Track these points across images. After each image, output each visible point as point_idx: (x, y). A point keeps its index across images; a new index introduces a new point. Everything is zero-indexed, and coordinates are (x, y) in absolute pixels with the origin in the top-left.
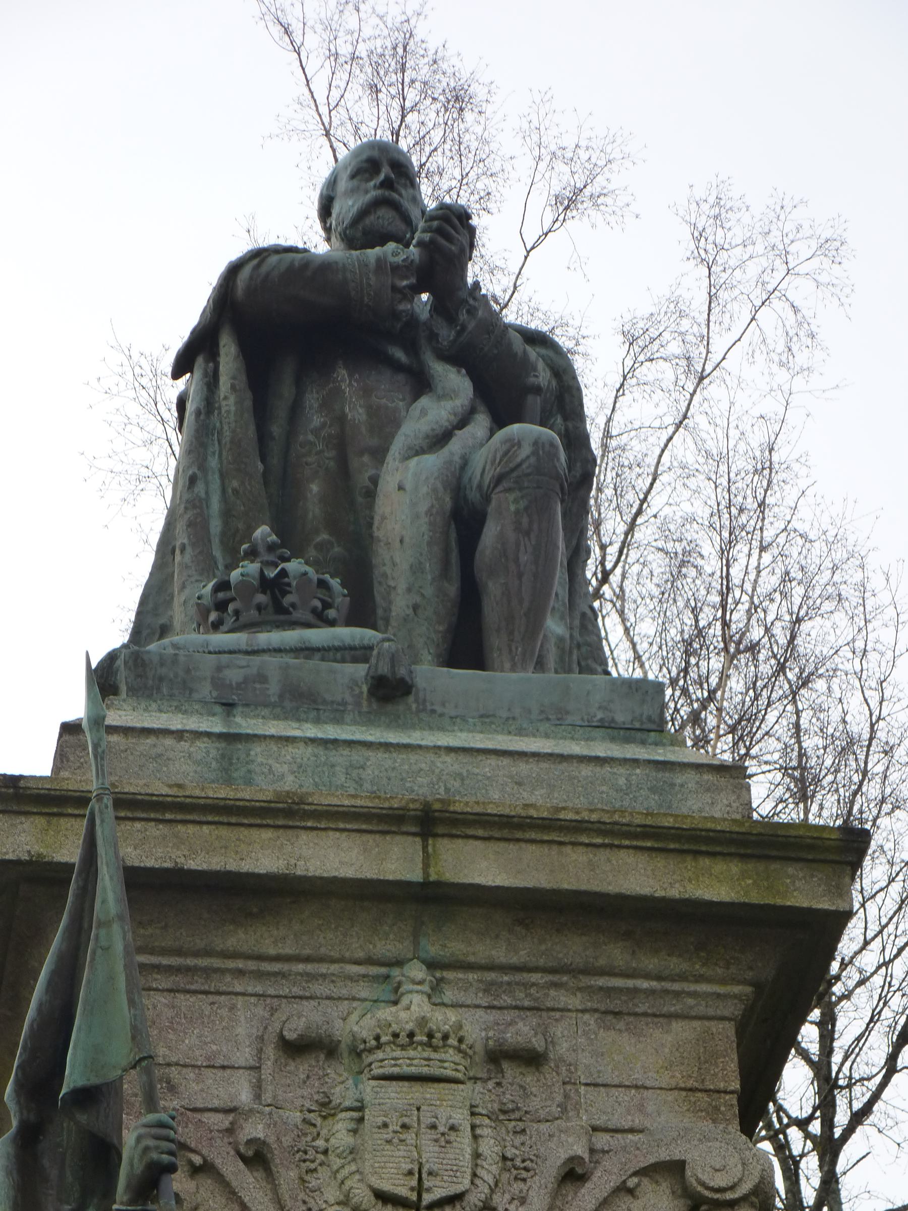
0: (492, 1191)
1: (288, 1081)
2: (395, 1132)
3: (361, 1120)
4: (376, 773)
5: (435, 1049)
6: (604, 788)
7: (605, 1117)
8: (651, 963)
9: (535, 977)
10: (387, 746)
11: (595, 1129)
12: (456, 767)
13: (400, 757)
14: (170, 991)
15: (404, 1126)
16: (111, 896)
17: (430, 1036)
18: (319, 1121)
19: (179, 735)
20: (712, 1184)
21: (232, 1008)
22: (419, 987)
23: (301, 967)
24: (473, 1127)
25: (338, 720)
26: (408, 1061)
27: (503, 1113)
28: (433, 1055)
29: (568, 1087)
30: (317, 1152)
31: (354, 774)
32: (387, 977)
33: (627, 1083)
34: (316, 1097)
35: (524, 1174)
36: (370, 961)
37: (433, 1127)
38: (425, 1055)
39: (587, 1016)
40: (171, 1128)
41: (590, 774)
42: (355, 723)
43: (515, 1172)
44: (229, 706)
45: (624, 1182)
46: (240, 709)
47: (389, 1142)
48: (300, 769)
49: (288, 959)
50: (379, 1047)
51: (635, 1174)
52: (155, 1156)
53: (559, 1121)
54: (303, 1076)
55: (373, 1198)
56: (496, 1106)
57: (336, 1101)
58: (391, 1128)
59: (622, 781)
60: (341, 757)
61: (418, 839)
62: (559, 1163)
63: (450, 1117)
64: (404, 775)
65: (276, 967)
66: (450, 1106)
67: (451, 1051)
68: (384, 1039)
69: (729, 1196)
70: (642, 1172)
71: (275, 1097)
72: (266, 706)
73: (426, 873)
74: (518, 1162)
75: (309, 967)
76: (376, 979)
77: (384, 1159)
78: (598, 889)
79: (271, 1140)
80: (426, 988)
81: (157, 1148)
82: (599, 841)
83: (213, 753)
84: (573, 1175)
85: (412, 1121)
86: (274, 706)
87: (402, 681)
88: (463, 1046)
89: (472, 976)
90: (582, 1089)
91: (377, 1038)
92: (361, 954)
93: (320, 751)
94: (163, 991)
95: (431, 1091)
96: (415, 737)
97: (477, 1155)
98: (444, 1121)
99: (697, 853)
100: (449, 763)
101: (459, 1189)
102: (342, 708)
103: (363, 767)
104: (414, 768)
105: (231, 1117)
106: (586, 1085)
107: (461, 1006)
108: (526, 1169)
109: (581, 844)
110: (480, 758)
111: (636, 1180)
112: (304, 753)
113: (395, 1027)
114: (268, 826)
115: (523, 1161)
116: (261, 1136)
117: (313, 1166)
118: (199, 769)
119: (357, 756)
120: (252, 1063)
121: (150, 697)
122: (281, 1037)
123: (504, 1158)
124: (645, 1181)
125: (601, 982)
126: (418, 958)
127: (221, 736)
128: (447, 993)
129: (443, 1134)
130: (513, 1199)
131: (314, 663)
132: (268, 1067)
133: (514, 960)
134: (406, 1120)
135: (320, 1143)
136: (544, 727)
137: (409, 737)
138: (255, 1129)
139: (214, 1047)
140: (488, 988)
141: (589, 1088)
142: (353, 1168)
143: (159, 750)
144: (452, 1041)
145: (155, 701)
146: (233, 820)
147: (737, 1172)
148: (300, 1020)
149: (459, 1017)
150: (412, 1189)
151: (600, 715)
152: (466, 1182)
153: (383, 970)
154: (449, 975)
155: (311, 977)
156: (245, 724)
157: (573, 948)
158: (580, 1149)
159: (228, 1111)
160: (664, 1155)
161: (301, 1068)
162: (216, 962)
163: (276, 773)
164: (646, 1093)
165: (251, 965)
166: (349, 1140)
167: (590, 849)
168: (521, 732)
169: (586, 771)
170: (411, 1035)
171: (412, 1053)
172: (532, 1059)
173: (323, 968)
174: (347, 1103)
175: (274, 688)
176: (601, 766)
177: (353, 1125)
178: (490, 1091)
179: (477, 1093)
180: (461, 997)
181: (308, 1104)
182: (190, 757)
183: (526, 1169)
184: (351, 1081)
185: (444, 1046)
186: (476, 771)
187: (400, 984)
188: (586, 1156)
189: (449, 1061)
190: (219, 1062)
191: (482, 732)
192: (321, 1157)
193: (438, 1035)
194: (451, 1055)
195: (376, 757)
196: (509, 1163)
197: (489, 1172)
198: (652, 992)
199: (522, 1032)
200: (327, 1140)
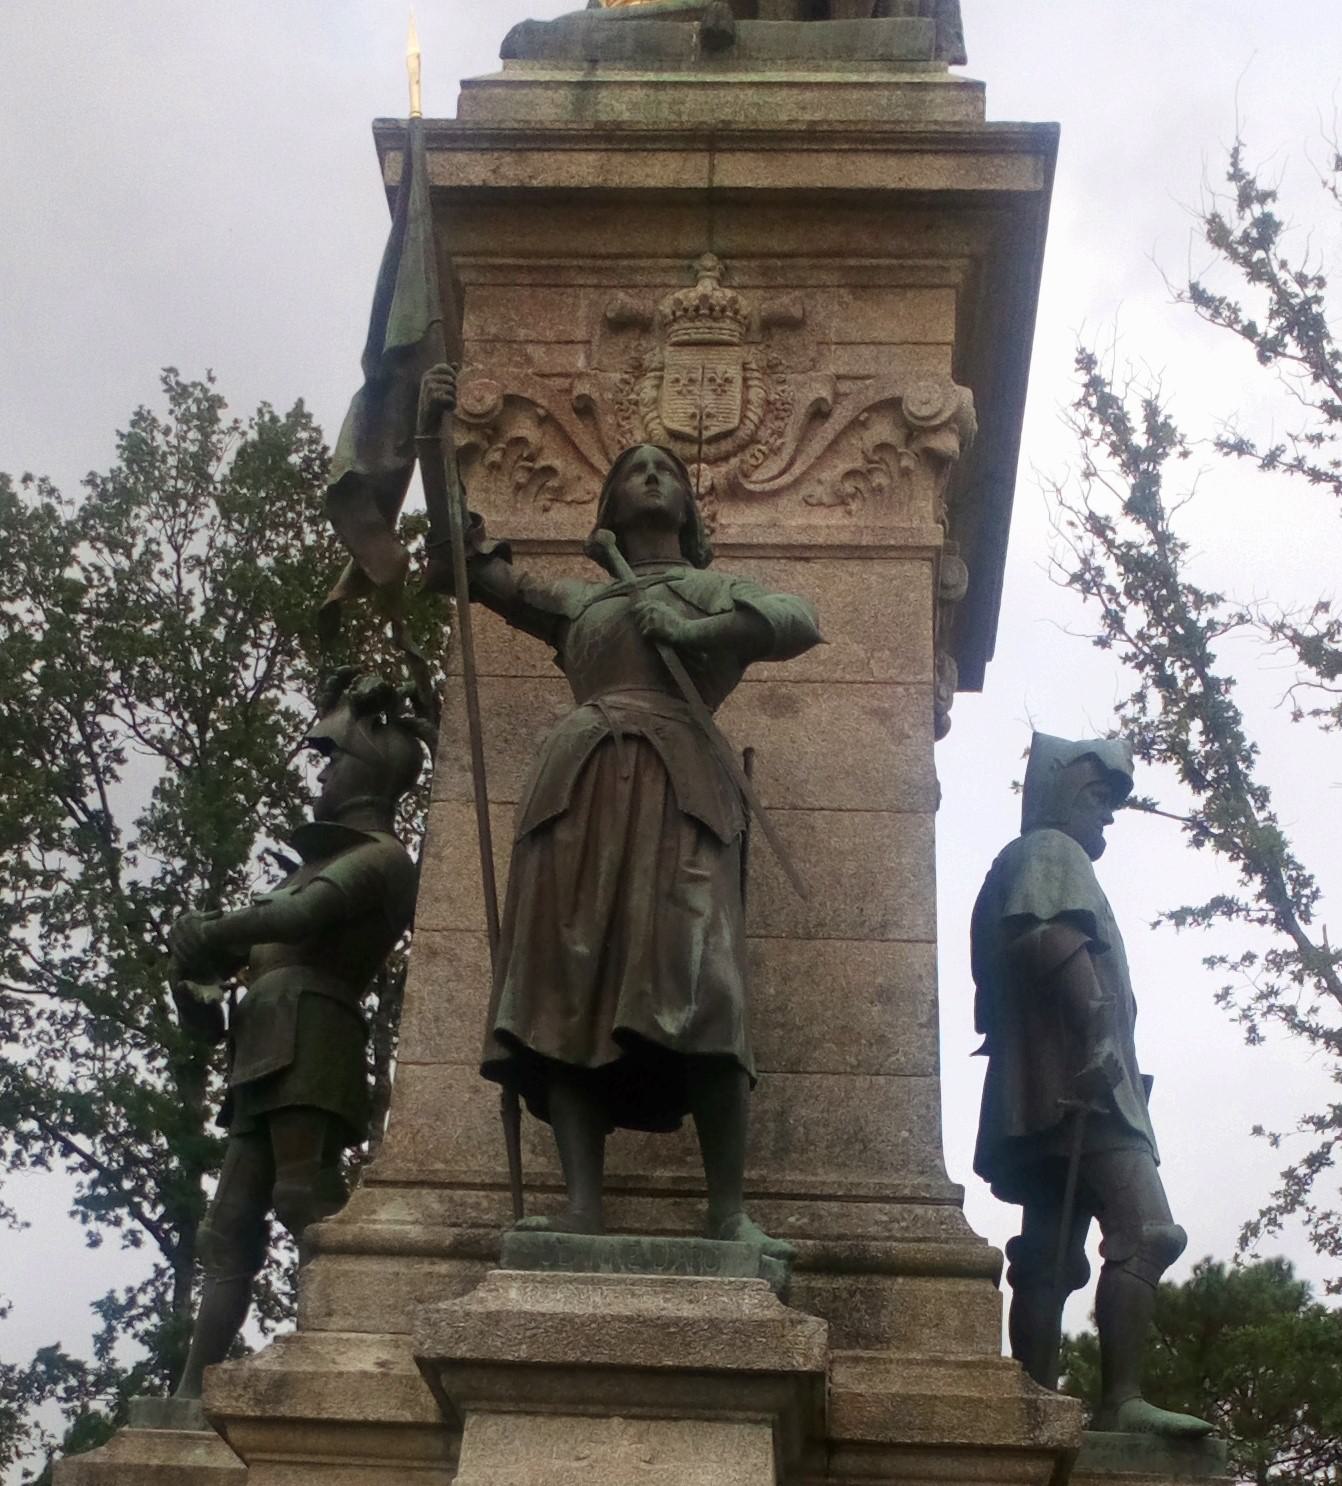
0: (757, 428)
3: (661, 378)
5: (715, 320)
8: (892, 244)
10: (704, 85)
11: (839, 377)
12: (756, 99)
13: (711, 93)
15: (692, 381)
17: (711, 309)
19: (546, 85)
20: (919, 414)
21: (577, 297)
23: (625, 263)
24: (745, 380)
25: (676, 69)
27: (770, 368)
31: (676, 108)
32: (690, 267)
35: (783, 414)
36: (677, 255)
37: (712, 380)
39: (842, 291)
42: (689, 69)
46: (602, 64)
47: (679, 393)
48: (634, 106)
50: (675, 320)
51: (864, 410)
56: (765, 363)
57: (646, 364)
59: (884, 102)
60: (665, 96)
61: (706, 154)
65: (608, 263)
66: (727, 364)
68: (678, 313)
69: (937, 422)
71: (599, 363)
72: (621, 59)
73: (711, 180)
74: (778, 405)
75: (632, 262)
79: (595, 396)
82: (846, 146)
83: (570, 97)
84: (819, 413)
89: (754, 263)
90: (833, 347)
91: (674, 313)
92: (668, 250)
93: (651, 92)
95: (714, 353)
96: (732, 77)
97: (746, 402)
99: (922, 152)
100: (750, 95)
101: (731, 426)
104: (723, 100)
105: (569, 381)
109: (835, 150)
112: (639, 94)
119: (677, 94)
120: (586, 338)
121: (535, 58)
123: (768, 403)
124: (874, 415)
125: (852, 262)
127: (579, 84)
131: (668, 23)
132: (596, 340)
134: (693, 376)
135: (633, 396)
136: (836, 64)
138: (583, 388)
140: (765, 272)
142: (655, 414)
143: (531, 96)
146: (567, 146)
147: (937, 405)
148: (623, 300)
150: (695, 428)
152: (736, 421)
153: (686, 262)
154: (735, 263)
155: (633, 270)
156: (601, 75)
157: (831, 236)
158: (825, 393)
159: (567, 375)
160: (887, 395)
161: (621, 341)
163: (616, 107)
164: (882, 348)
165: (589, 262)
166: (654, 393)
169: (855, 95)
170: (697, 309)
171: (698, 324)
172: (791, 324)
174: (653, 366)
177: (655, 382)
179: (752, 355)
181: (624, 367)
187: (697, 272)
188: (830, 399)
189: (727, 329)
190: (564, 338)
194: (727, 324)
195: (692, 95)
198: (890, 268)
199: (786, 303)
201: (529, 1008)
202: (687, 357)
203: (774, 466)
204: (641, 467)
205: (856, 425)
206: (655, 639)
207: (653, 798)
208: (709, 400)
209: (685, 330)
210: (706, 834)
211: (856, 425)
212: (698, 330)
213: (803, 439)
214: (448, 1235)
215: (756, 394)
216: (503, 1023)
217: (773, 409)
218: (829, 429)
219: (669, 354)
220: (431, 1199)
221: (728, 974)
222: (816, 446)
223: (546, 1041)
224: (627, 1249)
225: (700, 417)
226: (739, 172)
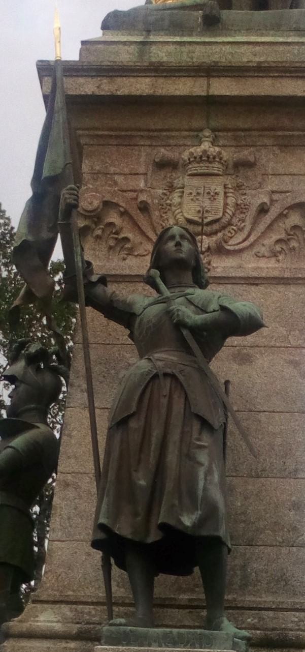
0: (232, 217)
1: (157, 178)
2: (194, 196)
3: (183, 192)
4: (199, 54)
5: (210, 163)
6: (288, 55)
7: (278, 187)
9: (254, 133)
10: (204, 43)
11: (273, 192)
13: (208, 47)
14: (117, 145)
16: (59, 100)
17: (208, 157)
18: (168, 193)
21: (140, 151)
22: (207, 139)
24: (225, 193)
25: (190, 35)
26: (200, 168)
28: (210, 165)
29: (264, 176)
30: (167, 205)
32: (197, 136)
33: (287, 173)
34: (167, 184)
35: (245, 211)
36: (190, 130)
37: (209, 193)
38: (207, 165)
39: (274, 148)
40: (76, 190)
41: (283, 49)
43: (241, 210)
44: (148, 32)
45: (282, 212)
47: (192, 200)
48: (169, 54)
49: (161, 130)
50: (190, 163)
51: (286, 209)
52: (68, 201)
53: (259, 189)
54: (163, 176)
55: (186, 222)
57: (175, 185)
58: (193, 195)
59: (296, 52)
60: (185, 49)
61: (206, 78)
62: (257, 205)
63: (216, 189)
64: (210, 54)
65: (156, 134)
66: (216, 185)
67: (217, 163)
68: (191, 159)
70: (288, 208)
74: (242, 206)
76: (193, 136)
77: (190, 207)
78: (277, 94)
79: (149, 201)
80: (211, 139)
81: (67, 193)
84: (263, 210)
85: (201, 191)
86: (166, 30)
87: (215, 16)
88: (222, 161)
89: (230, 134)
90: (270, 177)
91: (189, 159)
92: (186, 127)
93: (178, 47)
94: (114, 145)
96: (219, 39)
97: (226, 204)
98: (213, 191)
100: (228, 48)
101: (218, 217)
102: (192, 30)
103: (194, 52)
104: (214, 51)
106: (272, 175)
107: (225, 146)
108: (245, 209)
110: (241, 45)
111: (287, 211)
112: (171, 48)
113: (195, 154)
114: (147, 76)
115: (245, 206)
116: (145, 199)
117: (165, 211)
118: (131, 57)
120: (145, 172)
122: (154, 160)
123: (237, 205)
124: (291, 211)
125: (280, 133)
126: (208, 128)
128: (221, 142)
129: (212, 196)
130: (240, 221)
132: (150, 173)
133: (246, 126)
134: (199, 191)
135: (168, 202)
136: (271, 32)
137: (200, 39)
138: (143, 197)
139: (132, 167)
140: (235, 138)
141: (273, 176)
142: (180, 210)
144: (217, 159)
145: (120, 31)
148: (164, 152)
149: (220, 150)
150: (200, 218)
151: (294, 26)
152: (221, 214)
153: (196, 133)
154: (221, 134)
155: (169, 137)
156: (152, 38)
157: (269, 120)
158: (266, 200)
159: (135, 191)
162: (134, 133)
163: (160, 54)
164: (295, 177)
166: (179, 200)
167: (274, 78)
168: (262, 35)
169: (281, 48)
170: (201, 157)
171: (202, 165)
173: (174, 134)
174: (179, 186)
175: (167, 23)
176: (289, 46)
177: (180, 194)
178: (233, 179)
179: (230, 181)
180: (226, 142)
181: (164, 187)
182: (128, 52)
183: (245, 209)
184: (181, 178)
185: (214, 161)
186: (238, 51)
189: (216, 167)
190: (133, 172)
191: (246, 36)
192: (169, 207)
193: (211, 157)
194: (216, 165)
195: (198, 48)
196: (239, 207)
197: (230, 210)
199: (246, 154)
200: (171, 201)
201: (115, 513)
202: (196, 182)
203: (240, 237)
204: (173, 237)
205: (282, 216)
206: (180, 325)
207: (178, 406)
208: (207, 204)
209: (195, 168)
210: (205, 424)
211: (282, 216)
212: (202, 168)
213: (255, 223)
214: (74, 629)
215: (231, 200)
216: (102, 520)
217: (240, 208)
218: (268, 219)
219: (187, 180)
220: (66, 610)
221: (217, 495)
222: (261, 227)
223: (124, 529)
224: (166, 636)
225: (202, 212)
226: (223, 87)
